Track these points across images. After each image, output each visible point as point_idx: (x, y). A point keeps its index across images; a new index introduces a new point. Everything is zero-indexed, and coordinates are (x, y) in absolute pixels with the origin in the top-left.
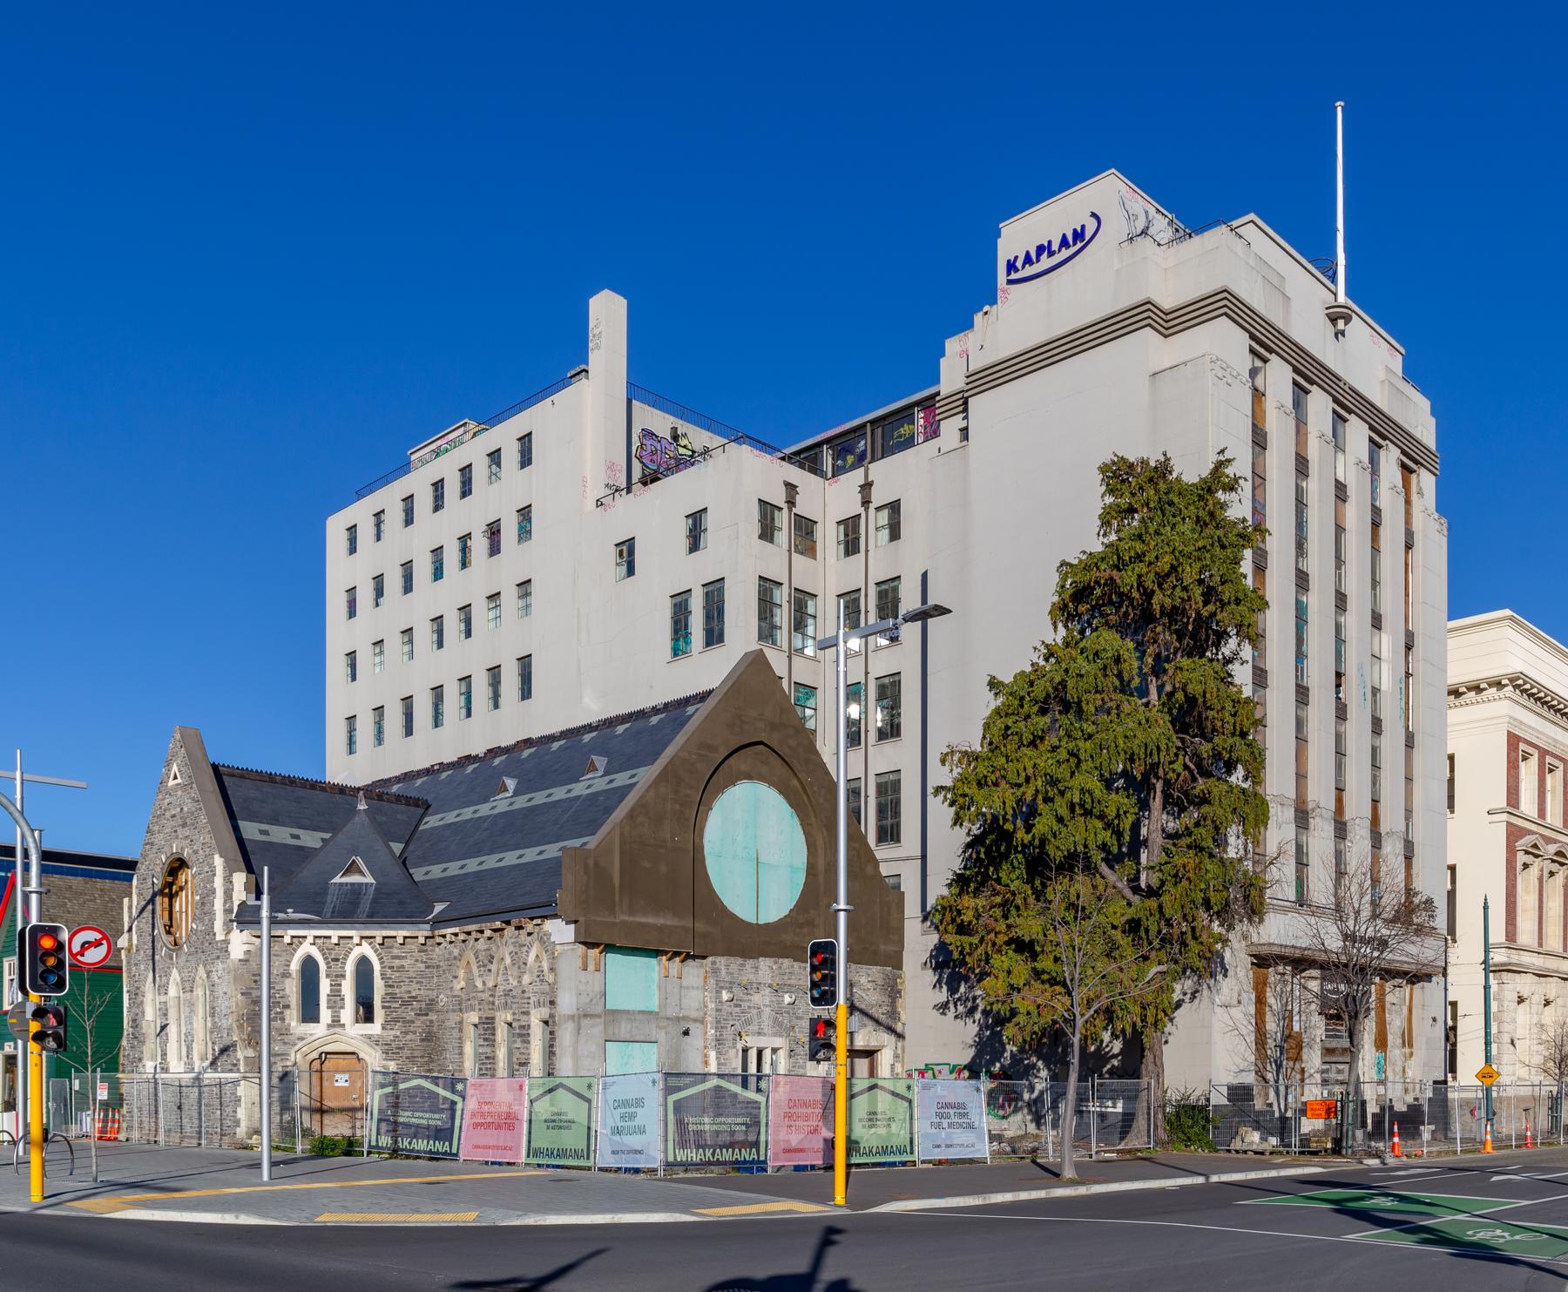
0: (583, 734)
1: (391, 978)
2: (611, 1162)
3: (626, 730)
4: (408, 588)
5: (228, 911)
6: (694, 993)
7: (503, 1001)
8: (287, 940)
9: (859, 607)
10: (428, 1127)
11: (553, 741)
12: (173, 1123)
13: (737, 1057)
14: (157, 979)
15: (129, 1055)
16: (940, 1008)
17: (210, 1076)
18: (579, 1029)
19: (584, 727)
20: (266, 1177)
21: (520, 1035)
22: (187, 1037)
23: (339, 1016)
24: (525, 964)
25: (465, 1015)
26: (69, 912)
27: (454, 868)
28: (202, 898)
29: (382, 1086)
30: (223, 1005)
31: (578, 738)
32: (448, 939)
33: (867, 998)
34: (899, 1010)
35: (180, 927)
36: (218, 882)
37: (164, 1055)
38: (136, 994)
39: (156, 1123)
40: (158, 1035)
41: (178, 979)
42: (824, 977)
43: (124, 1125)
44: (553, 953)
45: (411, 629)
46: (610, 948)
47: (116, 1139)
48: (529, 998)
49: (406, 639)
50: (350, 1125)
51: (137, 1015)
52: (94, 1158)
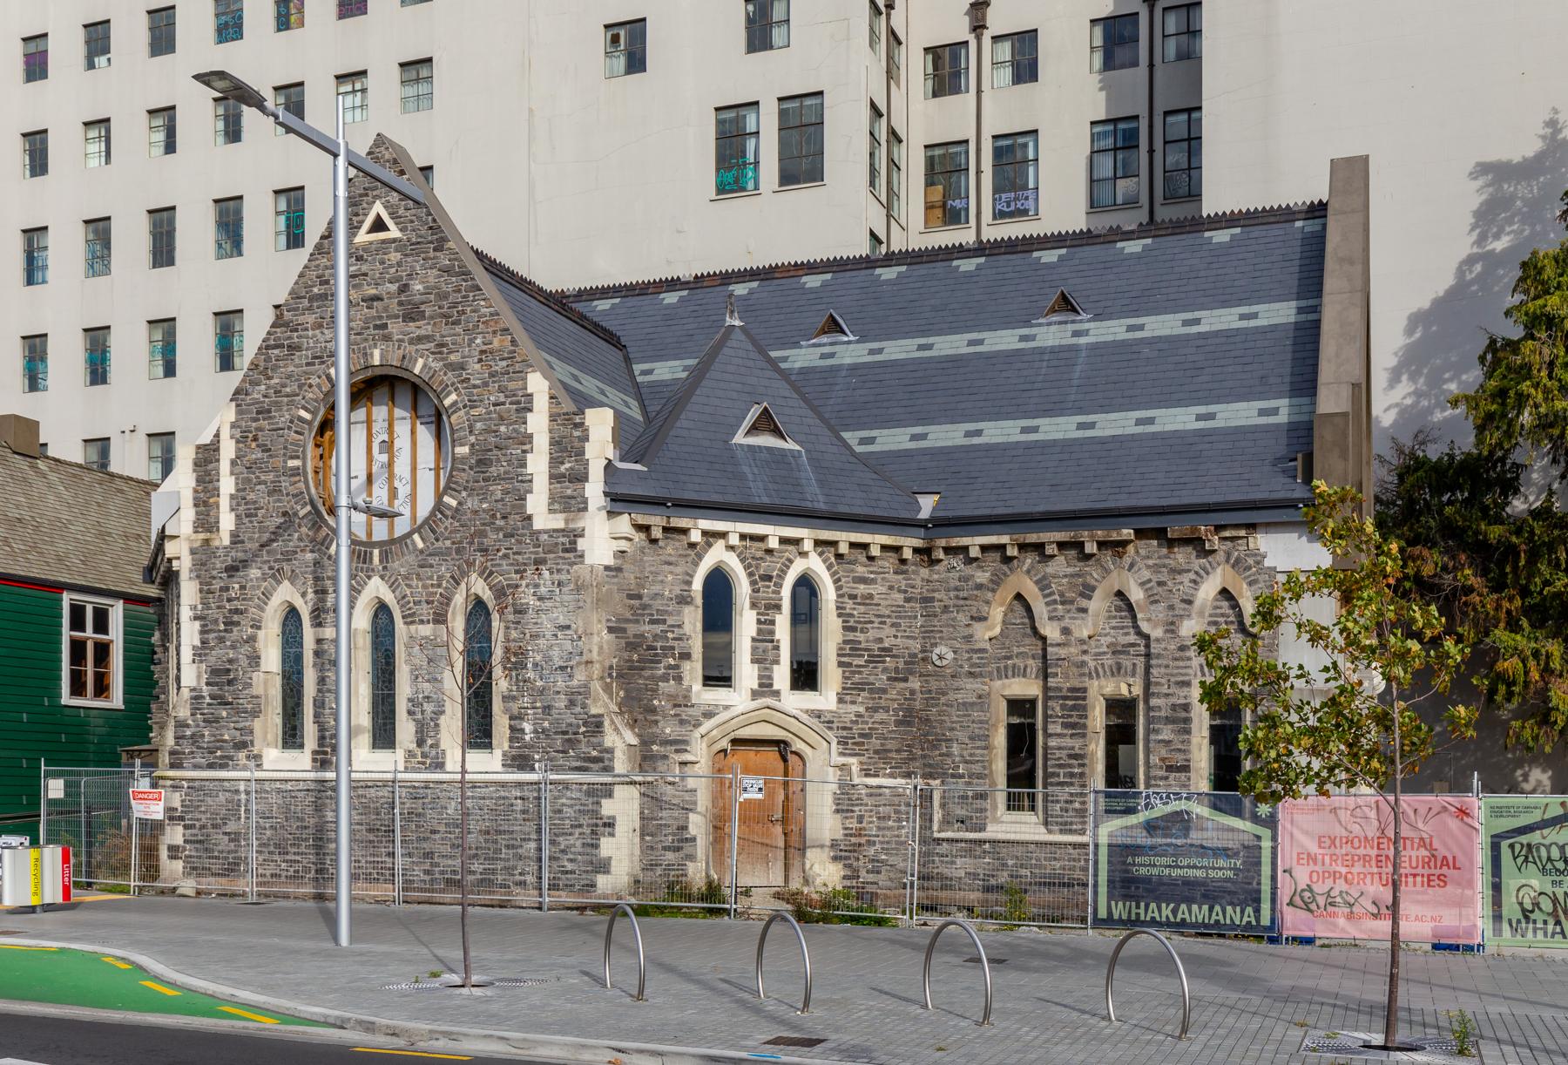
1: (852, 615)
8: (695, 536)
23: (770, 678)
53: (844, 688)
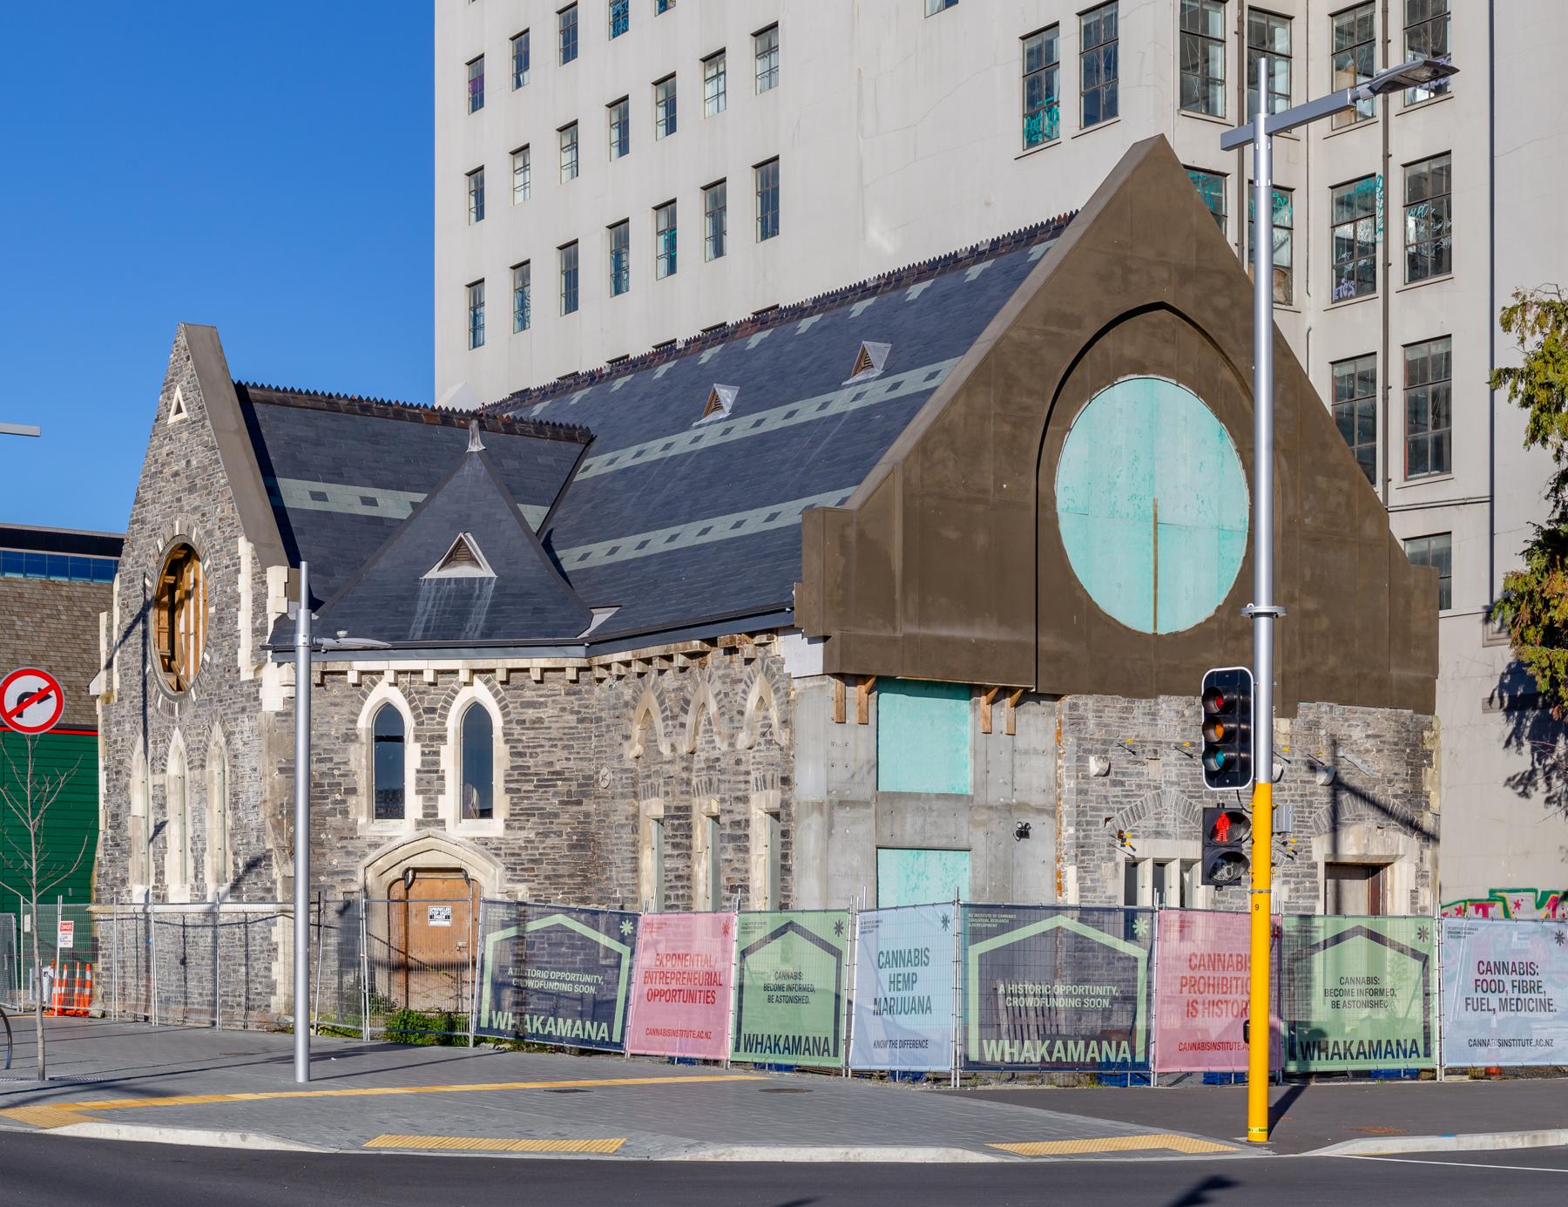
0: (852, 302)
1: (520, 741)
2: (883, 1060)
3: (926, 291)
4: (569, 51)
5: (259, 631)
6: (1037, 762)
7: (705, 779)
8: (352, 678)
9: (1371, 33)
10: (581, 998)
11: (801, 317)
12: (173, 988)
13: (1116, 876)
14: (151, 746)
15: (106, 874)
16: (1519, 783)
17: (230, 909)
18: (830, 826)
19: (853, 289)
20: (301, 1077)
21: (733, 838)
22: (194, 843)
23: (435, 807)
24: (741, 713)
25: (643, 804)
26: (18, 637)
27: (628, 548)
28: (220, 610)
29: (505, 925)
30: (252, 790)
31: (844, 309)
32: (614, 671)
33: (1361, 766)
34: (1427, 788)
35: (185, 659)
36: (244, 583)
37: (160, 873)
38: (119, 771)
39: (147, 987)
40: (152, 839)
41: (182, 746)
42: (1228, 736)
43: (99, 990)
44: (788, 694)
45: (575, 123)
46: (885, 683)
47: (86, 1013)
48: (748, 773)
49: (567, 141)
50: (452, 993)
51: (119, 806)
52: (40, 1041)
53: (512, 815)
